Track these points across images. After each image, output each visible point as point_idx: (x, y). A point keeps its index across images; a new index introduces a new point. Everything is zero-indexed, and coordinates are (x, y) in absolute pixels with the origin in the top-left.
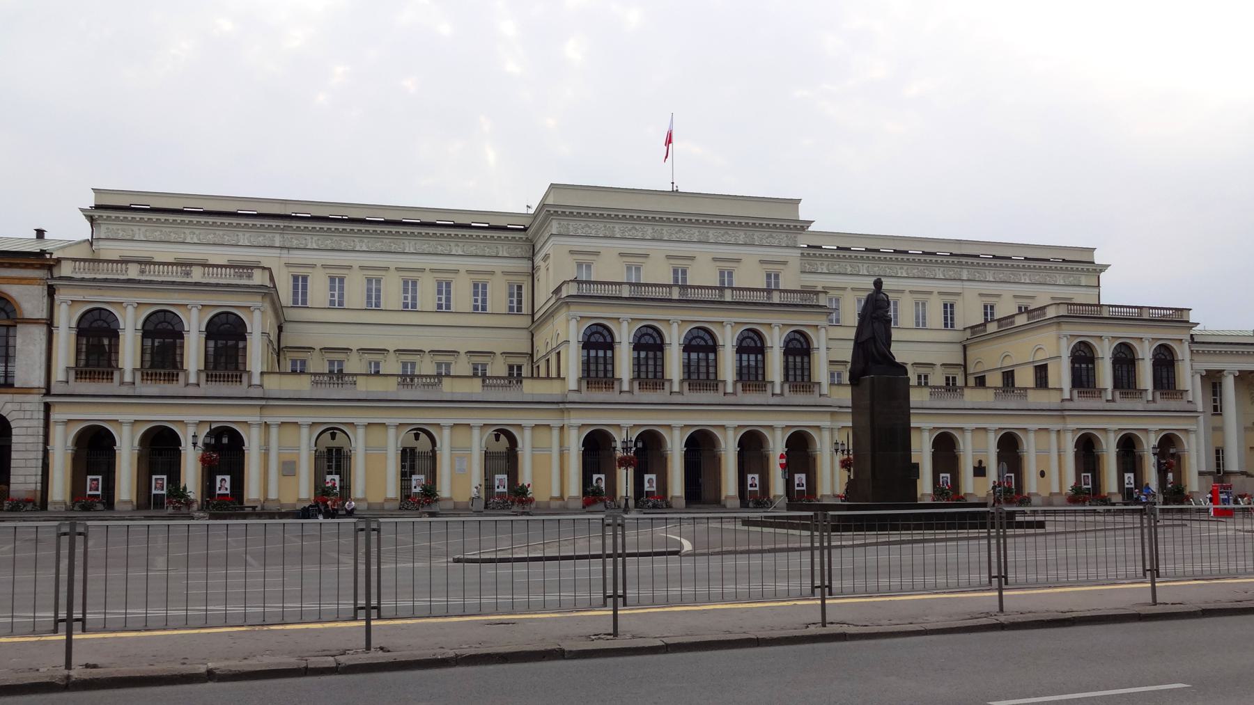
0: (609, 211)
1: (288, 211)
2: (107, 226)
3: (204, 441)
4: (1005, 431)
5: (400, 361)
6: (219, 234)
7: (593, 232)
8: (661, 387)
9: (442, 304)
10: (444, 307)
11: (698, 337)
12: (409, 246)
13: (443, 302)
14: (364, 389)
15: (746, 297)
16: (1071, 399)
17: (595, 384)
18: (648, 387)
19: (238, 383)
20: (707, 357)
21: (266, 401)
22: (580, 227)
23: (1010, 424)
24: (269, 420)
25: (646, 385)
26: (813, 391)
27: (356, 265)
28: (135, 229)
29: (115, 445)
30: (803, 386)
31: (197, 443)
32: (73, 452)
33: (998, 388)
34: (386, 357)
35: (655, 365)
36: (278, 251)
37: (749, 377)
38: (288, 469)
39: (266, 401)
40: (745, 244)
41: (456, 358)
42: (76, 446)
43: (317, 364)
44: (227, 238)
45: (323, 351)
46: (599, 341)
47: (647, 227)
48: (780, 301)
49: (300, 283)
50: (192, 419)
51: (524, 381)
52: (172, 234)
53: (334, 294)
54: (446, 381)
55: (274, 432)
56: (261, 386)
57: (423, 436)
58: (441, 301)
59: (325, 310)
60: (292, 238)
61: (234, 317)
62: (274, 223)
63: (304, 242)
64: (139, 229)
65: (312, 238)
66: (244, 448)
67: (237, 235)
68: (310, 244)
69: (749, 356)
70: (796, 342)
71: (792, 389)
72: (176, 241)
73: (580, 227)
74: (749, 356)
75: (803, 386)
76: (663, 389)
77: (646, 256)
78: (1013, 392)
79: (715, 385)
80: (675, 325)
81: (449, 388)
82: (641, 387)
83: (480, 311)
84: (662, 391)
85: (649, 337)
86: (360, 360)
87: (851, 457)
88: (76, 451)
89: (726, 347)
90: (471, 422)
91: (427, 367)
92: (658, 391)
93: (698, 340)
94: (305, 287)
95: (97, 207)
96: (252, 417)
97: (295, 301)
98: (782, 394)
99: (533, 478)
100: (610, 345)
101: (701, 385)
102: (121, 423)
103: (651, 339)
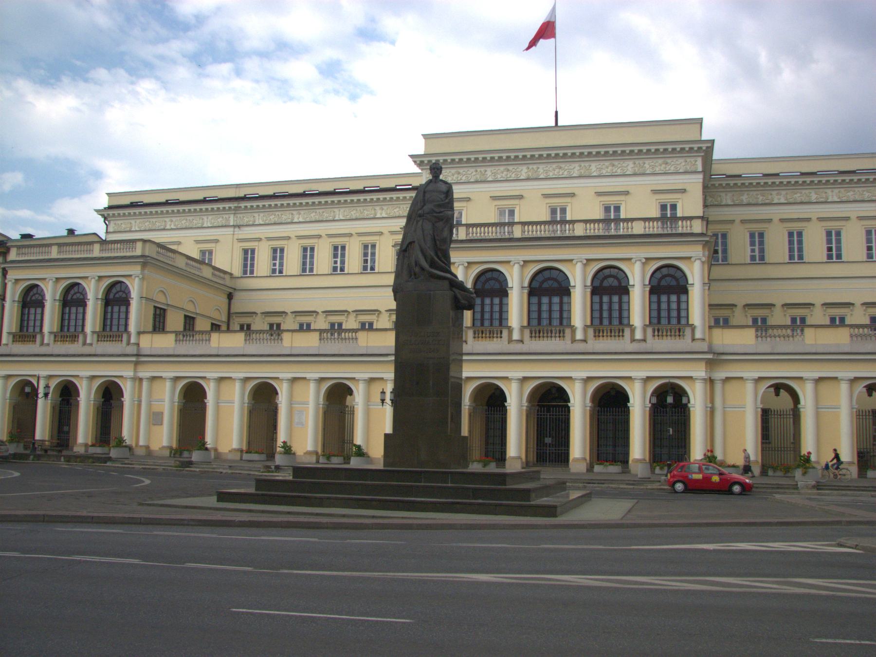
0: (437, 156)
1: (384, 184)
2: (115, 222)
3: (688, 397)
4: (259, 381)
5: (788, 315)
6: (805, 193)
7: (566, 173)
8: (499, 335)
9: (755, 255)
10: (338, 269)
11: (549, 279)
12: (339, 213)
13: (757, 253)
14: (365, 345)
15: (477, 233)
16: (521, 341)
17: (107, 337)
18: (484, 335)
19: (120, 342)
20: (601, 299)
21: (139, 358)
22: (604, 167)
23: (191, 372)
24: (141, 375)
25: (482, 334)
26: (684, 336)
27: (814, 217)
28: (829, 191)
29: (506, 402)
30: (671, 330)
31: (385, 400)
32: (182, 404)
33: (180, 332)
34: (254, 319)
35: (540, 311)
36: (232, 229)
37: (118, 328)
38: (156, 418)
39: (139, 358)
40: (635, 175)
41: (284, 318)
42: (327, 401)
43: (321, 323)
44: (325, 215)
45: (746, 307)
46: (553, 286)
47: (521, 167)
48: (645, 231)
49: (249, 256)
50: (811, 375)
51: (806, 330)
52: (865, 193)
53: (754, 249)
54: (808, 332)
55: (145, 384)
56: (138, 344)
57: (783, 392)
58: (754, 252)
59: (823, 265)
60: (323, 212)
61: (624, 275)
62: (227, 205)
63: (824, 195)
64: (832, 191)
65: (259, 215)
66: (506, 404)
67: (203, 219)
68: (134, 227)
69: (492, 301)
70: (493, 281)
71: (533, 335)
72: (763, 202)
73: (551, 169)
74: (492, 301)
75: (671, 330)
76: (501, 337)
77: (521, 197)
78: (272, 335)
79: (499, 332)
80: (517, 266)
81: (812, 339)
82: (476, 335)
83: (339, 272)
84: (499, 339)
85: (663, 280)
86: (785, 315)
87: (552, 409)
88: (184, 404)
89: (695, 285)
90: (632, 374)
91: (351, 323)
92: (495, 339)
93: (550, 282)
94: (800, 242)
95: (110, 208)
96: (128, 372)
97: (245, 272)
98: (644, 340)
99: (470, 431)
100: (623, 290)
101: (545, 332)
102: (358, 380)
103: (673, 280)
